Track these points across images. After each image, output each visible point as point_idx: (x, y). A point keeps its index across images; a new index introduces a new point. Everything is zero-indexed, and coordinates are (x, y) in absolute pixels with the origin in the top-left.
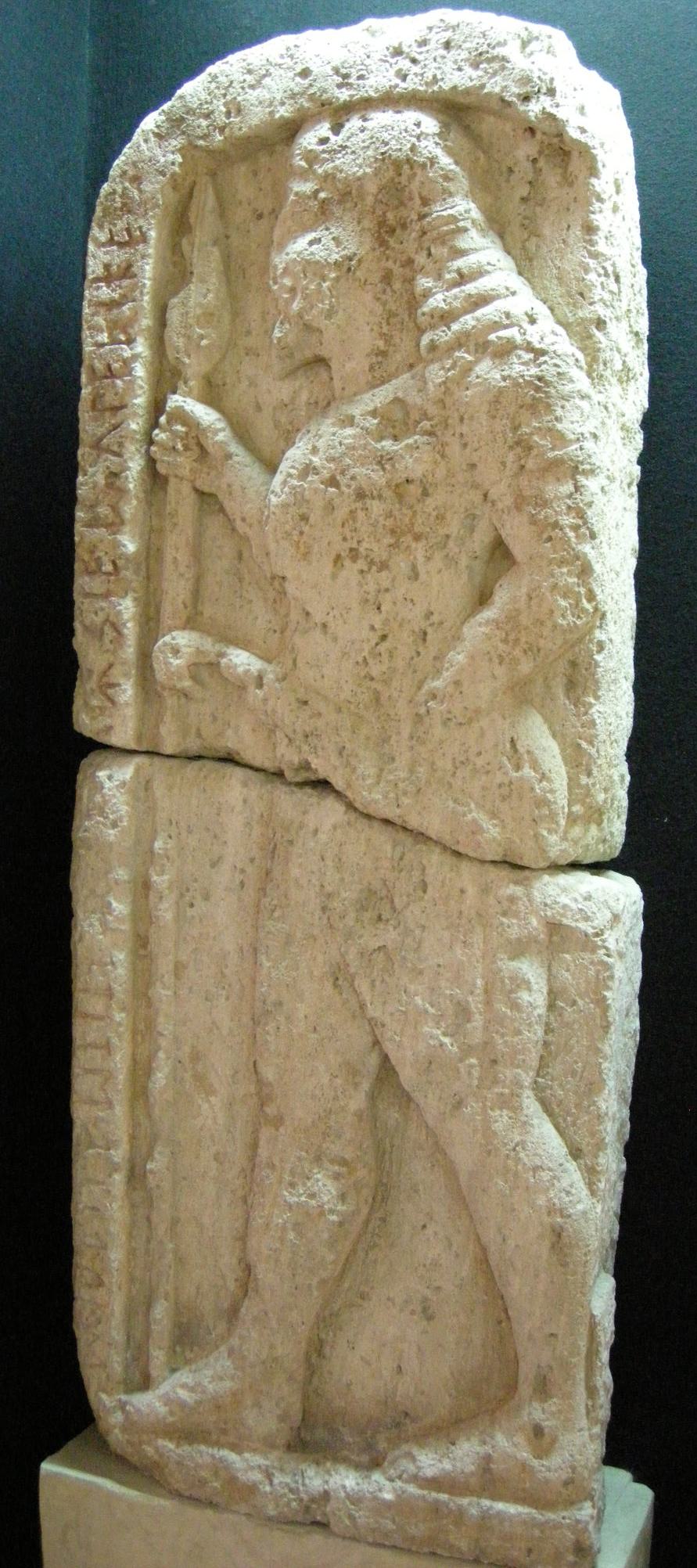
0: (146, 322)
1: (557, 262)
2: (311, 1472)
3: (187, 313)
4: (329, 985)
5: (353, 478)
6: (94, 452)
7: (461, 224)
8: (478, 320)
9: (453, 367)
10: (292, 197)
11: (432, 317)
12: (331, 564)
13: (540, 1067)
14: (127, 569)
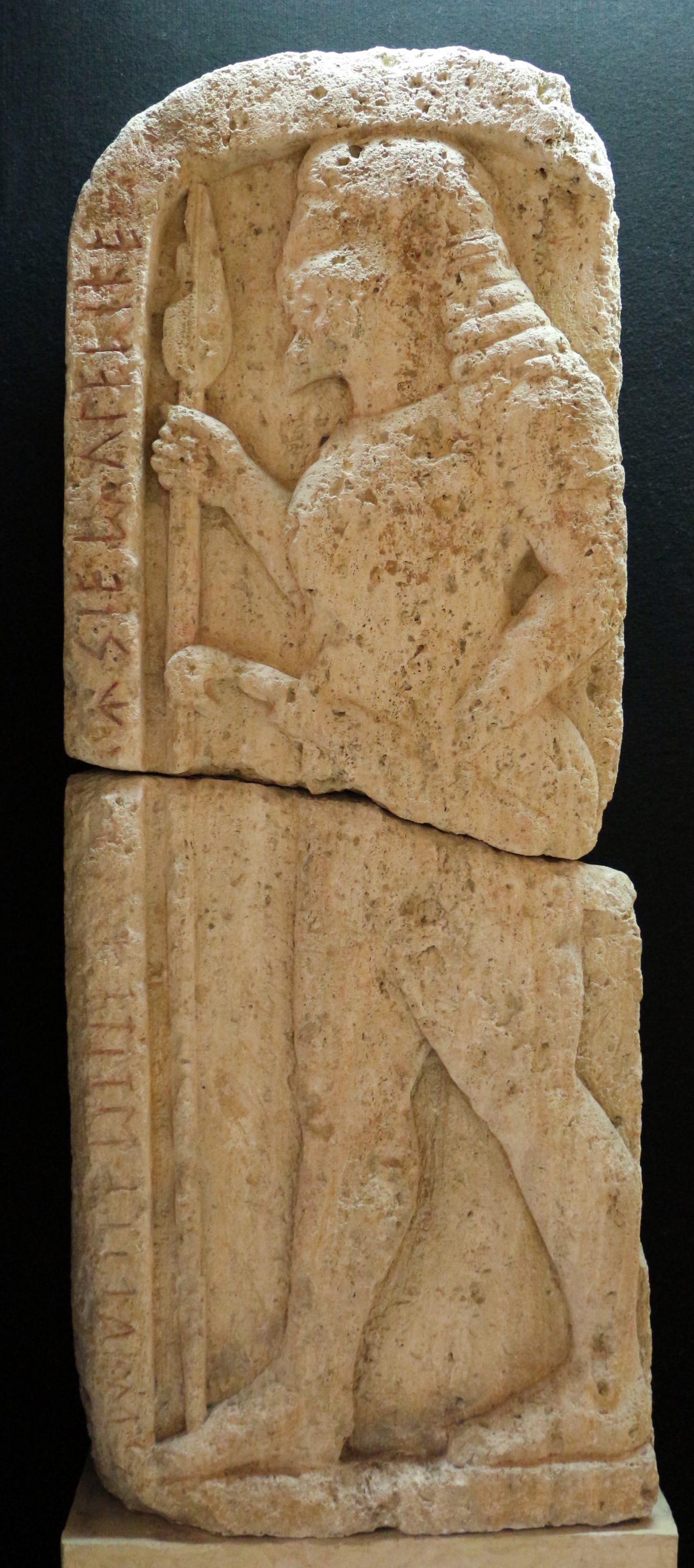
0: (142, 329)
1: (572, 297)
2: (376, 1477)
3: (189, 323)
4: (375, 990)
5: (390, 493)
6: (87, 462)
7: (491, 254)
8: (513, 345)
9: (490, 389)
10: (308, 214)
11: (467, 341)
12: (368, 576)
13: (580, 1045)
14: (129, 583)
